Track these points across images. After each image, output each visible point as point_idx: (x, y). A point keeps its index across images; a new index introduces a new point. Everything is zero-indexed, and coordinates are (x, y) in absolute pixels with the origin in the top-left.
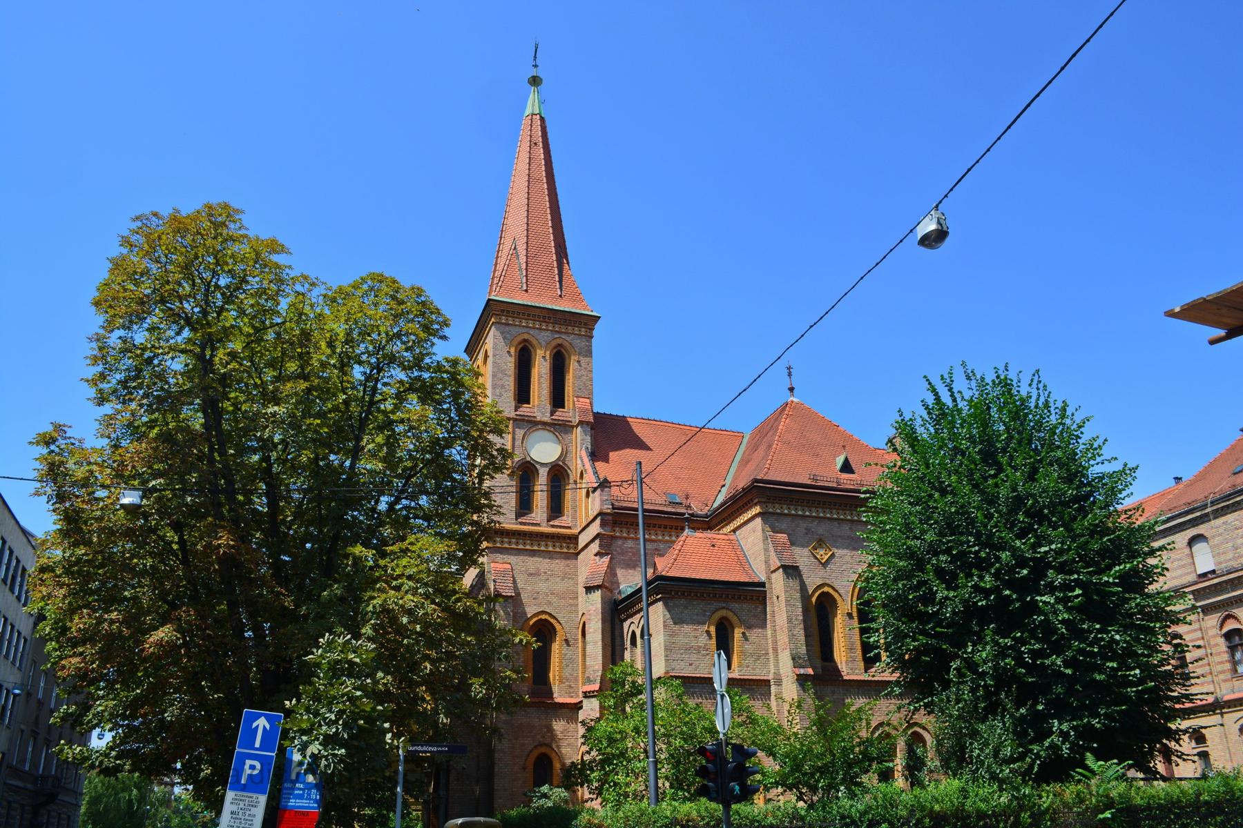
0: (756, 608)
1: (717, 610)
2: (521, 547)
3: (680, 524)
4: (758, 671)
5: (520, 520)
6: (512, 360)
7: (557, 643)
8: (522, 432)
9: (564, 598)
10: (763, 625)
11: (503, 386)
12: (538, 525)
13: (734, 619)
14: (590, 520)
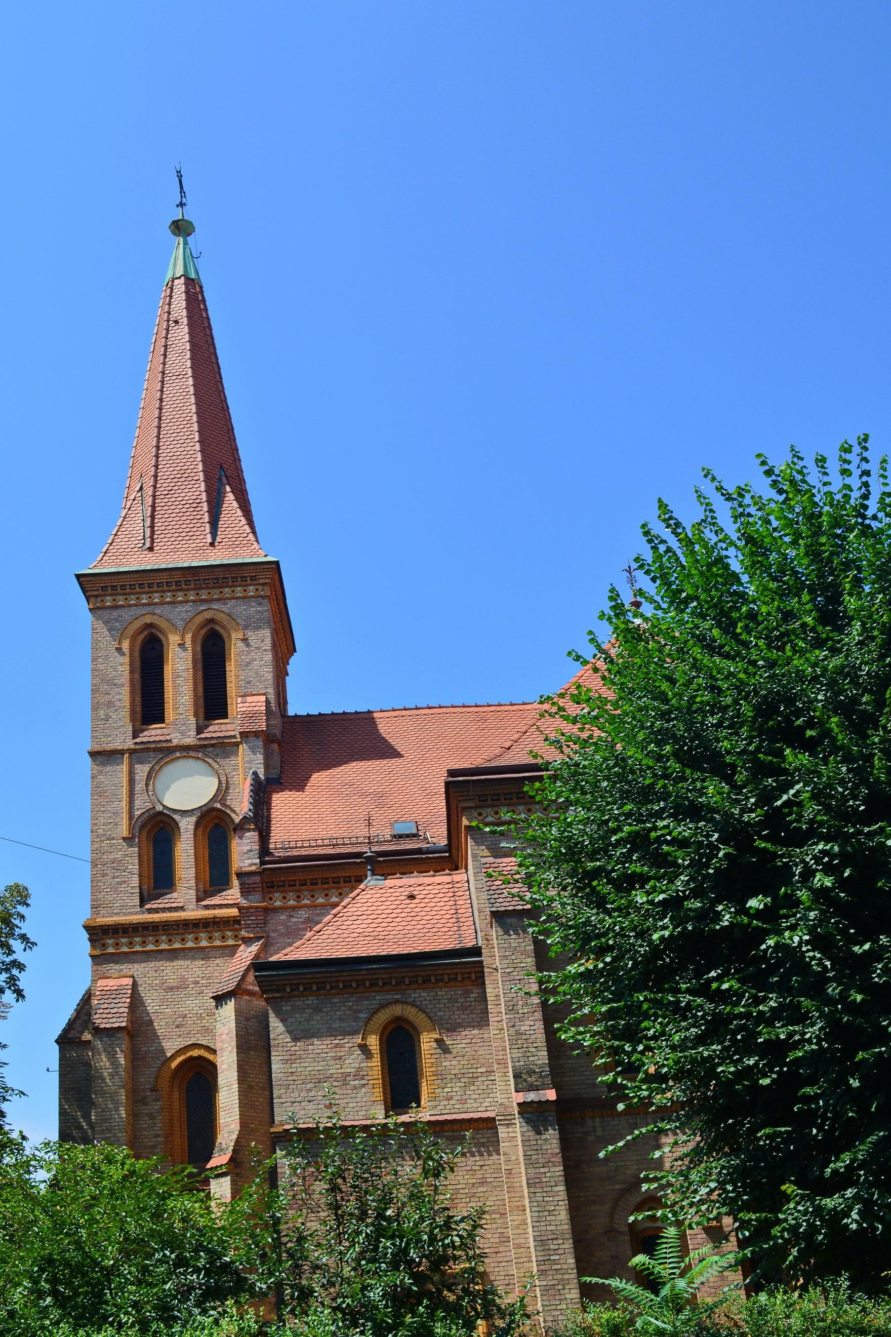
0: (467, 993)
1: (383, 1006)
2: (151, 947)
3: (357, 872)
4: (471, 1104)
5: (148, 906)
6: (126, 659)
8: (147, 768)
10: (482, 1020)
12: (182, 908)
13: (419, 1019)
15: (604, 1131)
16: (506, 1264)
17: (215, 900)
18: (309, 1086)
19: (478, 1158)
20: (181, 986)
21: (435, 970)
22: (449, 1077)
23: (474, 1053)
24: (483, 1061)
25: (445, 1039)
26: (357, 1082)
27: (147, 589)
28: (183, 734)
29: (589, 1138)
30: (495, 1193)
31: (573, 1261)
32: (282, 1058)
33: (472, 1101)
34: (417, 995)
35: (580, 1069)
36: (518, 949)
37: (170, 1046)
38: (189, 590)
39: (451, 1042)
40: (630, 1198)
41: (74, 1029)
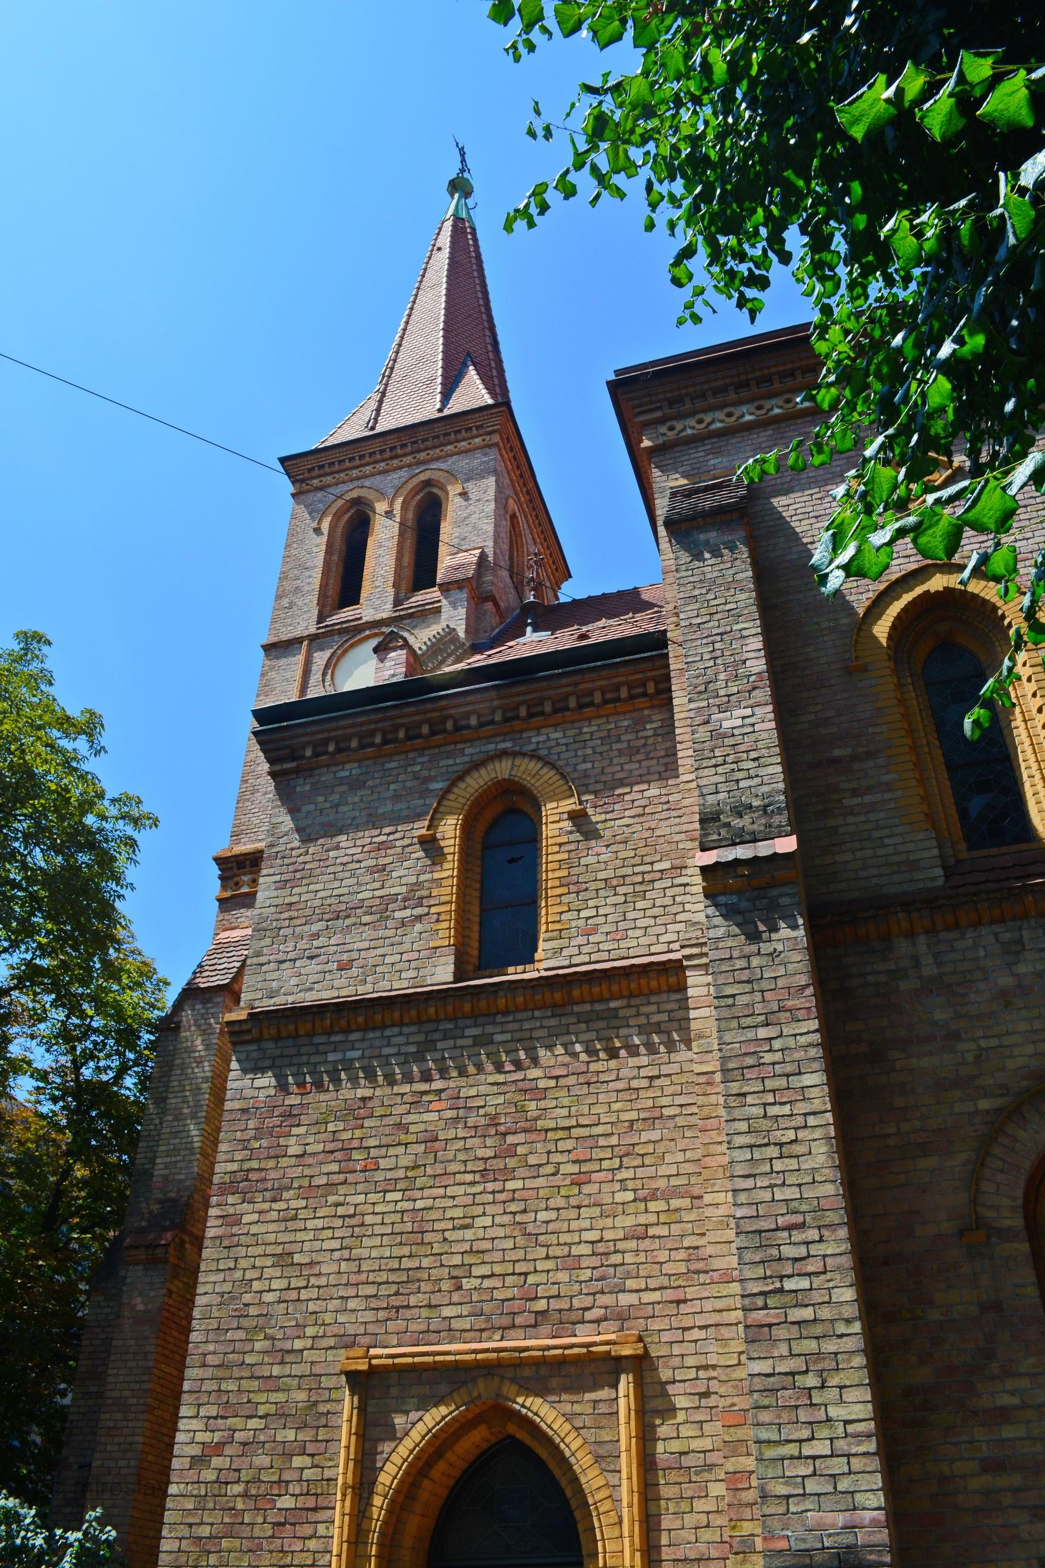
0: (639, 724)
1: (476, 766)
8: (328, 653)
10: (668, 768)
15: (939, 964)
16: (702, 1334)
18: (315, 928)
19: (644, 1060)
21: (576, 684)
22: (592, 886)
23: (648, 834)
24: (666, 847)
25: (590, 811)
26: (407, 913)
29: (904, 986)
30: (682, 1144)
31: (849, 1294)
32: (277, 878)
33: (639, 933)
34: (542, 738)
35: (875, 834)
36: (719, 581)
39: (603, 817)
40: (1021, 1134)
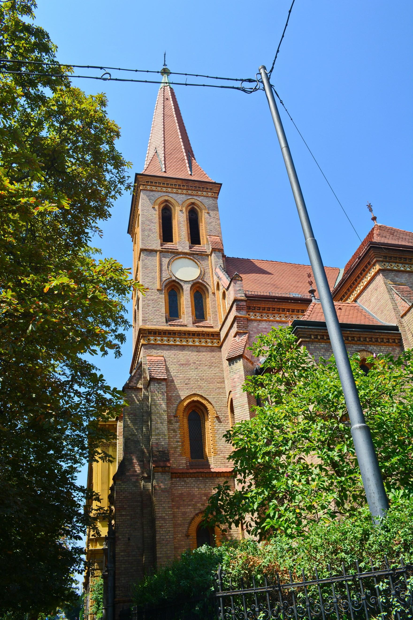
2: (172, 343)
6: (157, 213)
7: (210, 420)
8: (168, 260)
9: (212, 383)
11: (150, 230)
12: (186, 326)
14: (227, 311)
17: (201, 324)
20: (187, 364)
27: (166, 186)
28: (183, 247)
37: (183, 394)
38: (184, 189)
41: (132, 382)
